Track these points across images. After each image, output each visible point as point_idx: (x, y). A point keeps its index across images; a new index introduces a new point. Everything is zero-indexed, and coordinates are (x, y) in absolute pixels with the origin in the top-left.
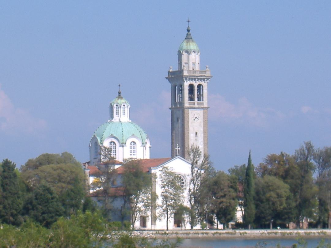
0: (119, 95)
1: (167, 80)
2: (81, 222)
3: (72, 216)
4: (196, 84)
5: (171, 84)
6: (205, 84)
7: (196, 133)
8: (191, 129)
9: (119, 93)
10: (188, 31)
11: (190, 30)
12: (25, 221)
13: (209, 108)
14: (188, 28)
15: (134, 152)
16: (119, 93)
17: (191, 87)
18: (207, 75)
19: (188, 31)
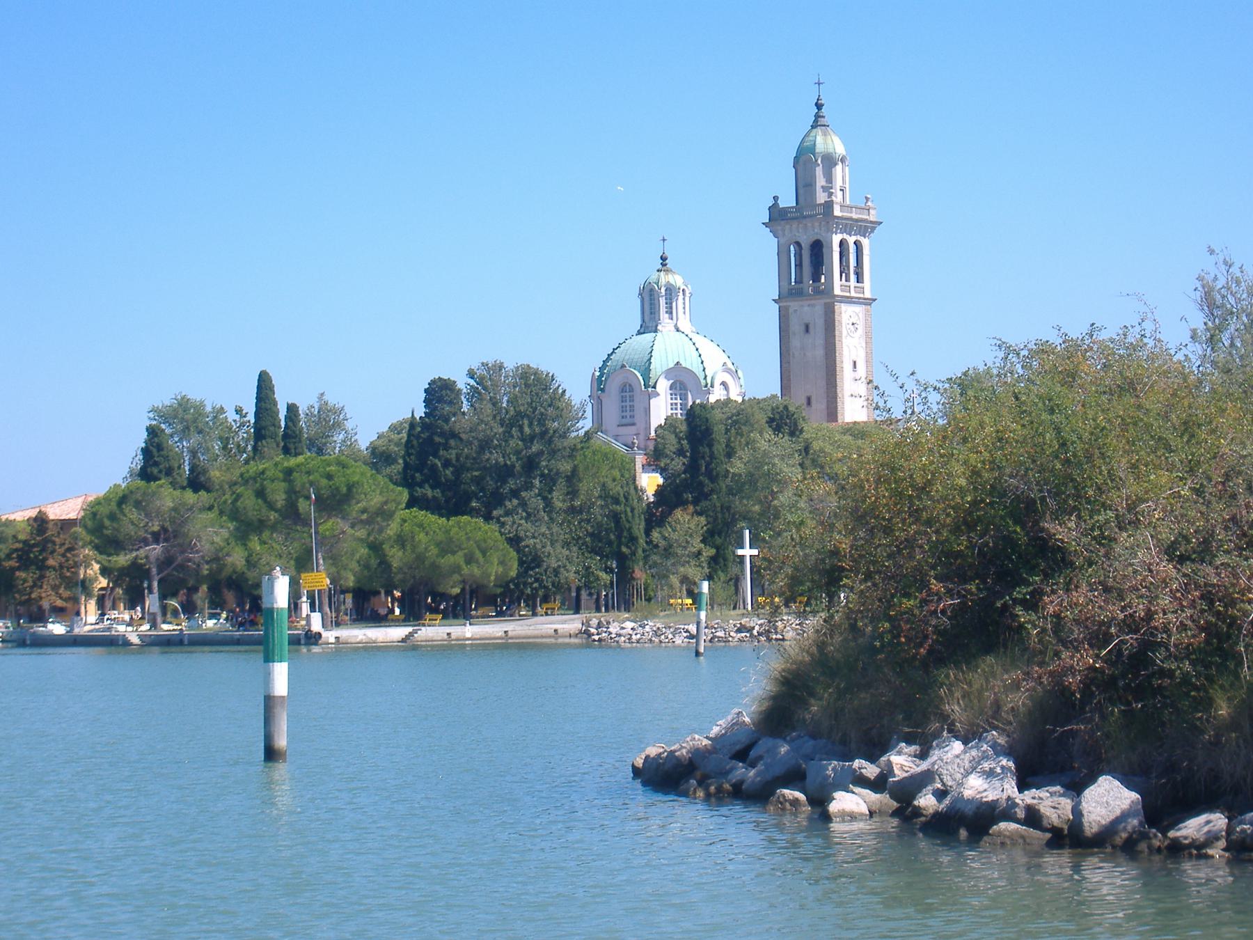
0: (663, 265)
1: (768, 229)
2: (500, 532)
3: (678, 902)
4: (851, 240)
5: (776, 239)
6: (865, 242)
7: (855, 362)
8: (845, 352)
9: (664, 259)
10: (819, 106)
11: (823, 105)
12: (376, 795)
13: (875, 300)
14: (818, 100)
15: (674, 407)
16: (664, 259)
17: (842, 244)
18: (872, 218)
19: (819, 106)
